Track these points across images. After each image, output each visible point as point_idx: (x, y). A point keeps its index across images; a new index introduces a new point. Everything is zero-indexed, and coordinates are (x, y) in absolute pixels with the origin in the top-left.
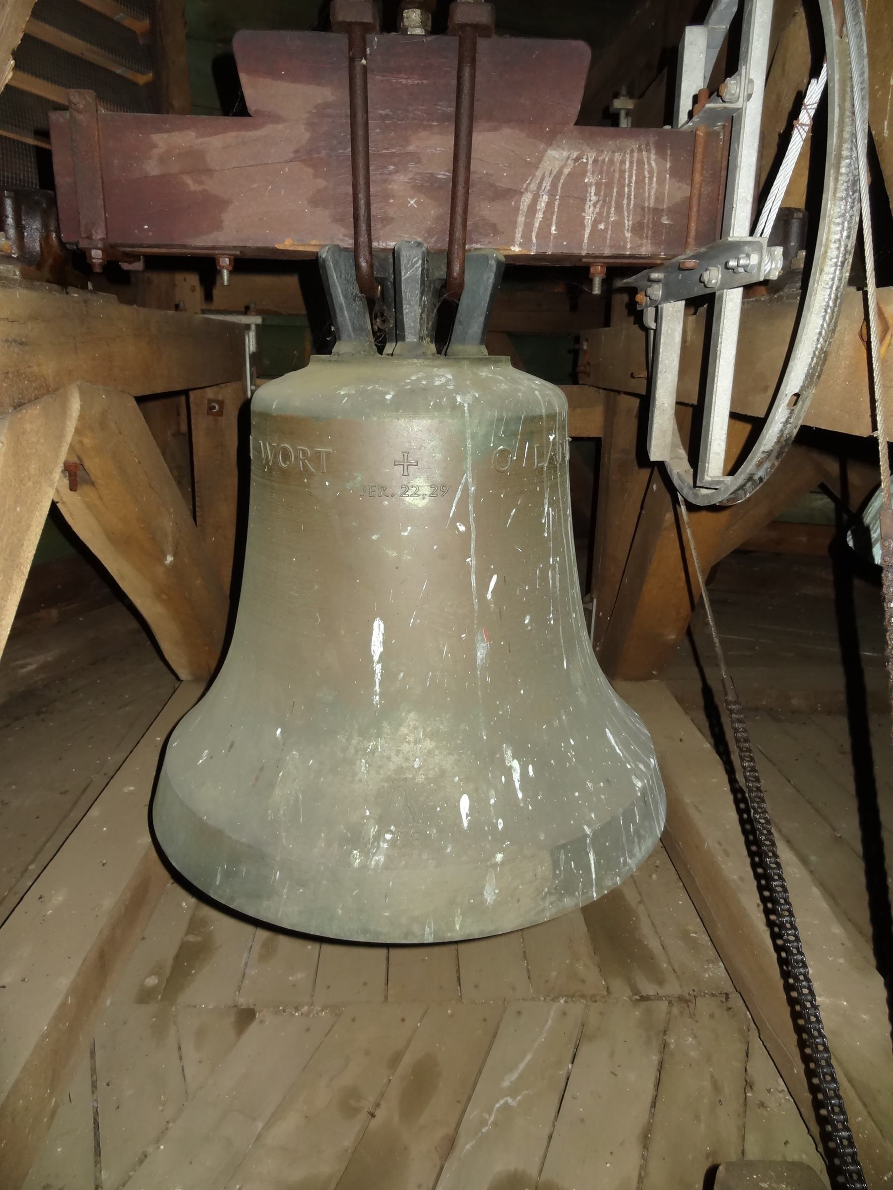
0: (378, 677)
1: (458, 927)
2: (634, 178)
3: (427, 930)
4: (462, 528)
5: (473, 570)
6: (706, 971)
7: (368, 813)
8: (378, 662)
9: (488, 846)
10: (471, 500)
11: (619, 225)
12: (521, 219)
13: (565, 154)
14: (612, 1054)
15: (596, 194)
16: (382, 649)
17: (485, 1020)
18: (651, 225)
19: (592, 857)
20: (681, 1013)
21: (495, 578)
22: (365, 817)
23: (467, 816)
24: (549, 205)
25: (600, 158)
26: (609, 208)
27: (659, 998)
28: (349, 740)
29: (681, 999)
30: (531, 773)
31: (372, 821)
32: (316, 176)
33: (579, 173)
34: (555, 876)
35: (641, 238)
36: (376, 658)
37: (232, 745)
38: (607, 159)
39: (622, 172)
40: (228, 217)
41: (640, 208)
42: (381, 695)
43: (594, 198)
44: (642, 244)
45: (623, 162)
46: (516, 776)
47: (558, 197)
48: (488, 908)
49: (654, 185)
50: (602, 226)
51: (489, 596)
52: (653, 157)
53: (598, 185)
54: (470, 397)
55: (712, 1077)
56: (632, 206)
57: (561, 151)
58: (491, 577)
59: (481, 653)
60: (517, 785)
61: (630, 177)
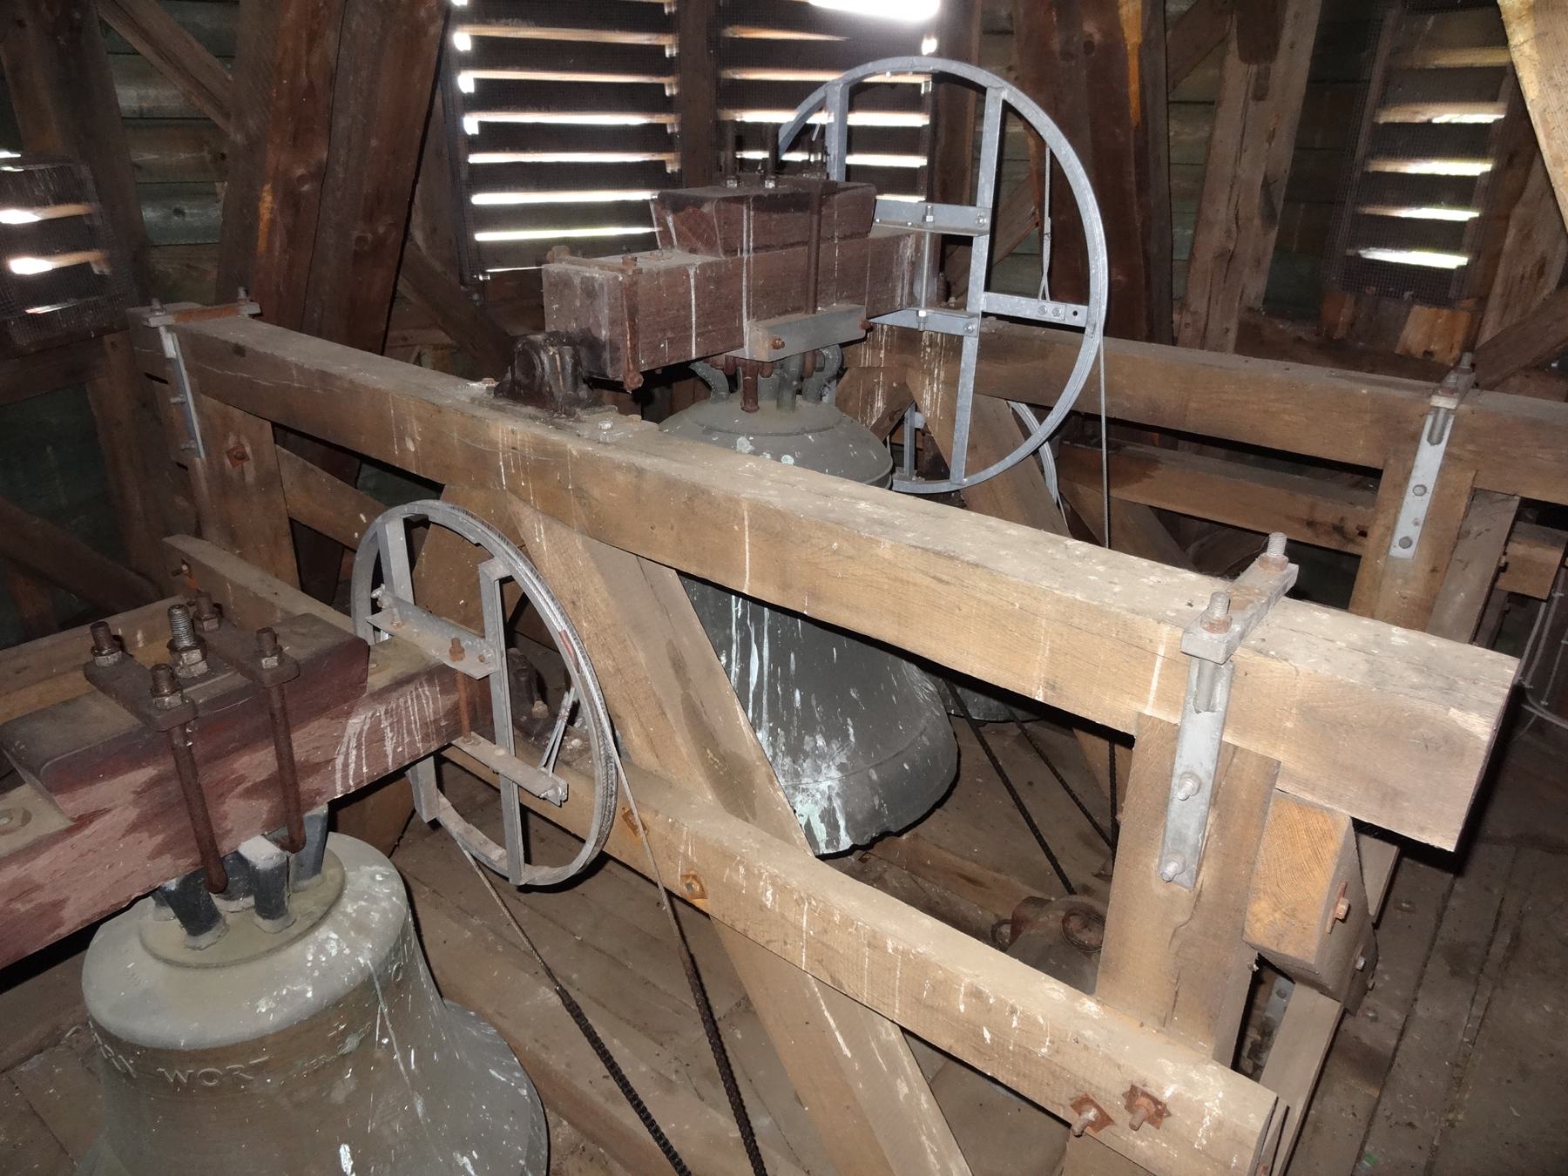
13: (363, 717)
24: (358, 757)
26: (403, 735)
30: (476, 1156)
39: (407, 708)
41: (425, 724)
43: (390, 735)
45: (406, 702)
51: (413, 1067)
52: (426, 688)
59: (420, 1109)
61: (413, 709)
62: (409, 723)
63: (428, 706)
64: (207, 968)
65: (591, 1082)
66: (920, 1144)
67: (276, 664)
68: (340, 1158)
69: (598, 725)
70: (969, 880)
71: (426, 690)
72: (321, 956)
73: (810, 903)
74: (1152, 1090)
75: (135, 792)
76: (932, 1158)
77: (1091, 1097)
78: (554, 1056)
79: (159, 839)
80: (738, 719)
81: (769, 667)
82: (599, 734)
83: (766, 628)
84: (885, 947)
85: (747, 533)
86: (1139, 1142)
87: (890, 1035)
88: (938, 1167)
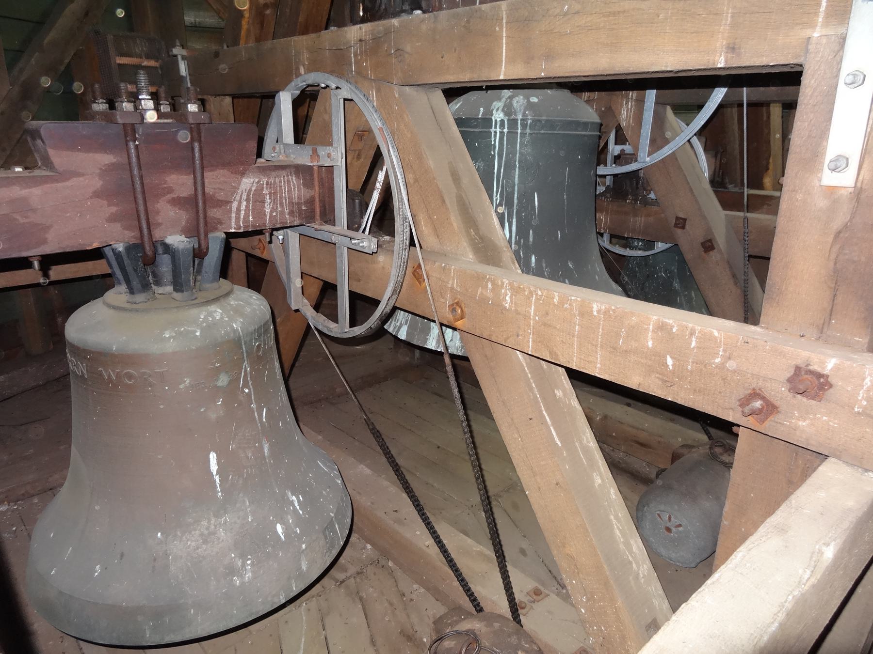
0: (218, 482)
1: (294, 589)
2: (287, 189)
3: (281, 597)
4: (247, 391)
5: (255, 410)
6: (363, 554)
7: (233, 555)
8: (216, 475)
9: (297, 544)
10: (249, 376)
11: (282, 213)
12: (234, 215)
13: (252, 180)
14: (341, 615)
15: (269, 199)
16: (217, 467)
17: (271, 635)
18: (297, 211)
19: (337, 526)
20: (362, 579)
21: (265, 409)
22: (232, 558)
23: (282, 533)
24: (247, 207)
25: (270, 181)
26: (277, 204)
27: (348, 578)
28: (209, 522)
29: (358, 573)
30: (301, 499)
31: (237, 558)
32: (109, 205)
33: (259, 191)
34: (327, 543)
35: (293, 217)
36: (215, 473)
37: (122, 555)
38: (272, 181)
39: (281, 187)
40: (51, 236)
41: (291, 203)
42: (221, 491)
43: (269, 201)
44: (294, 220)
45: (280, 182)
46: (296, 504)
47: (251, 202)
48: (305, 573)
49: (296, 192)
50: (274, 214)
51: (264, 420)
52: (294, 178)
53: (270, 194)
54: (239, 323)
55: (387, 600)
56: (287, 203)
57: (250, 179)
58: (263, 409)
59: (266, 450)
60: (298, 508)
61: (285, 189)
62: (281, 198)
63: (294, 191)
64: (137, 311)
65: (385, 513)
66: (610, 520)
67: (197, 110)
68: (210, 461)
69: (399, 193)
70: (642, 445)
71: (294, 179)
72: (209, 318)
73: (537, 294)
74: (815, 367)
75: (101, 169)
76: (618, 532)
77: (758, 391)
78: (364, 498)
79: (114, 209)
80: (493, 220)
81: (516, 238)
82: (400, 199)
83: (515, 211)
84: (592, 311)
85: (505, 29)
86: (800, 423)
87: (590, 443)
88: (622, 540)
